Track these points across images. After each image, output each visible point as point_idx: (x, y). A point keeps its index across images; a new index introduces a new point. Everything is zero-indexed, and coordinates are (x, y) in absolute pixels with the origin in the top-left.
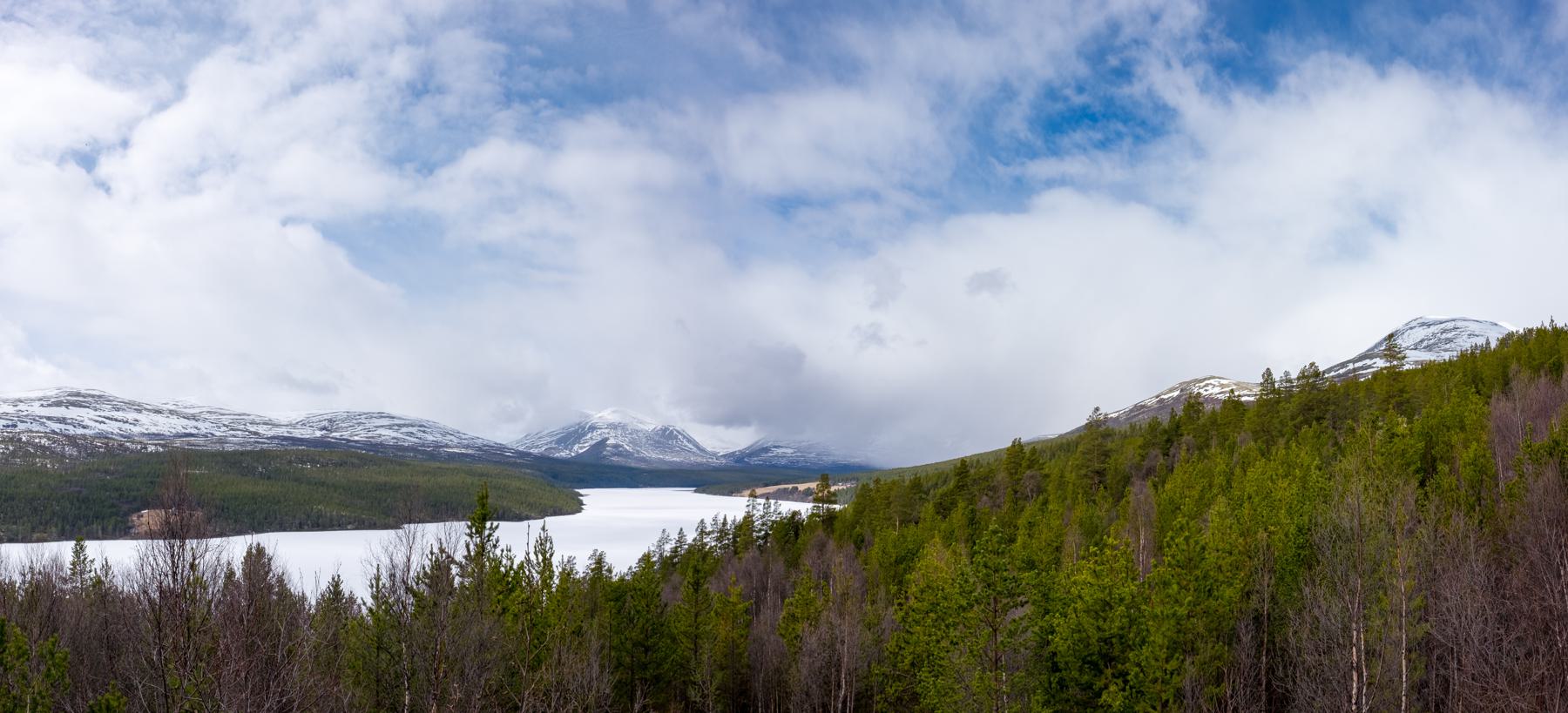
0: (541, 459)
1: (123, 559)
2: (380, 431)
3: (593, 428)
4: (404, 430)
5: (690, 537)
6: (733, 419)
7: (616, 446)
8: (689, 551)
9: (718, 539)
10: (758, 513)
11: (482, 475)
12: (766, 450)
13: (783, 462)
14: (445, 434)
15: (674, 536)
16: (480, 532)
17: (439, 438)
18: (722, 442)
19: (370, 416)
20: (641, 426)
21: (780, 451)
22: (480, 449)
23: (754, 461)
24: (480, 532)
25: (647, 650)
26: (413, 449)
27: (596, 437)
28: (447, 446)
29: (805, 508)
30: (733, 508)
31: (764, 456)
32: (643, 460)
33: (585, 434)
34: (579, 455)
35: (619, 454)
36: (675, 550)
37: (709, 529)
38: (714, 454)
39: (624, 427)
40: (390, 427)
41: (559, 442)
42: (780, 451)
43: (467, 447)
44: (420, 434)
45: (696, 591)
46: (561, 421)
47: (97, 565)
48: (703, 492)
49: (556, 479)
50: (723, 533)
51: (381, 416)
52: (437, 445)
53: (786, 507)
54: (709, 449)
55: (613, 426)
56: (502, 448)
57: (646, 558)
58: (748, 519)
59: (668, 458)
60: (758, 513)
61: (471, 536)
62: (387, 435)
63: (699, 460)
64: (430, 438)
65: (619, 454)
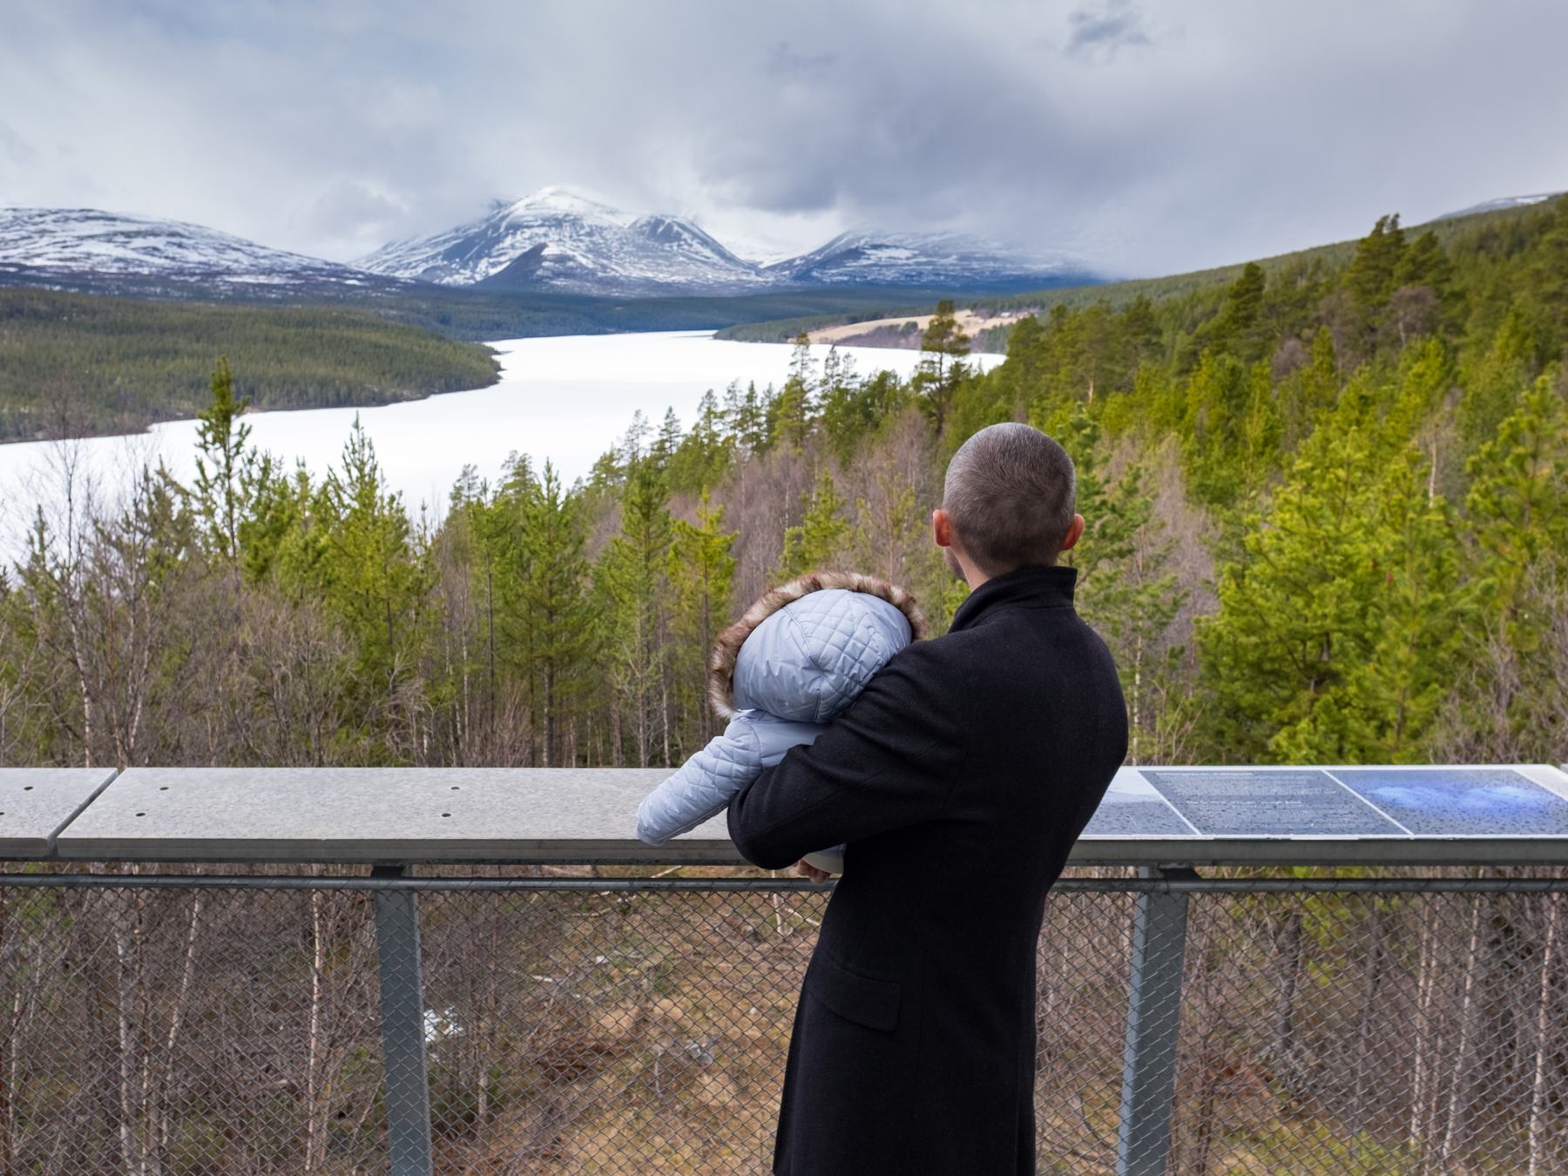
0: (422, 288)
1: (47, 287)
2: (88, 247)
3: (515, 227)
4: (138, 242)
5: (688, 421)
6: (807, 197)
7: (562, 259)
8: (684, 449)
9: (740, 425)
10: (815, 374)
11: (302, 324)
12: (855, 254)
13: (890, 275)
14: (223, 248)
15: (657, 421)
16: (221, 439)
17: (211, 256)
18: (766, 240)
19: (64, 217)
20: (606, 220)
21: (884, 254)
22: (295, 274)
23: (833, 275)
24: (221, 439)
25: (552, 612)
26: (161, 278)
27: (514, 247)
28: (229, 271)
29: (904, 363)
30: (764, 366)
31: (852, 265)
32: (614, 282)
33: (499, 240)
34: (488, 280)
35: (568, 274)
36: (661, 446)
37: (721, 408)
38: (753, 267)
39: (575, 222)
40: (109, 238)
41: (449, 255)
42: (876, 255)
43: (269, 272)
44: (172, 251)
45: (646, 516)
46: (463, 210)
47: (763, 668)
48: (731, 337)
49: (422, 335)
50: (748, 414)
51: (87, 216)
52: (210, 273)
53: (867, 364)
54: (742, 256)
55: (557, 222)
56: (340, 272)
57: (606, 465)
58: (796, 388)
59: (663, 277)
60: (815, 374)
61: (204, 447)
62: (104, 255)
63: (723, 276)
64: (193, 257)
65: (568, 274)
